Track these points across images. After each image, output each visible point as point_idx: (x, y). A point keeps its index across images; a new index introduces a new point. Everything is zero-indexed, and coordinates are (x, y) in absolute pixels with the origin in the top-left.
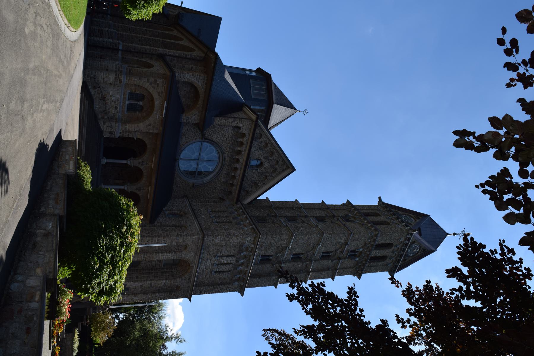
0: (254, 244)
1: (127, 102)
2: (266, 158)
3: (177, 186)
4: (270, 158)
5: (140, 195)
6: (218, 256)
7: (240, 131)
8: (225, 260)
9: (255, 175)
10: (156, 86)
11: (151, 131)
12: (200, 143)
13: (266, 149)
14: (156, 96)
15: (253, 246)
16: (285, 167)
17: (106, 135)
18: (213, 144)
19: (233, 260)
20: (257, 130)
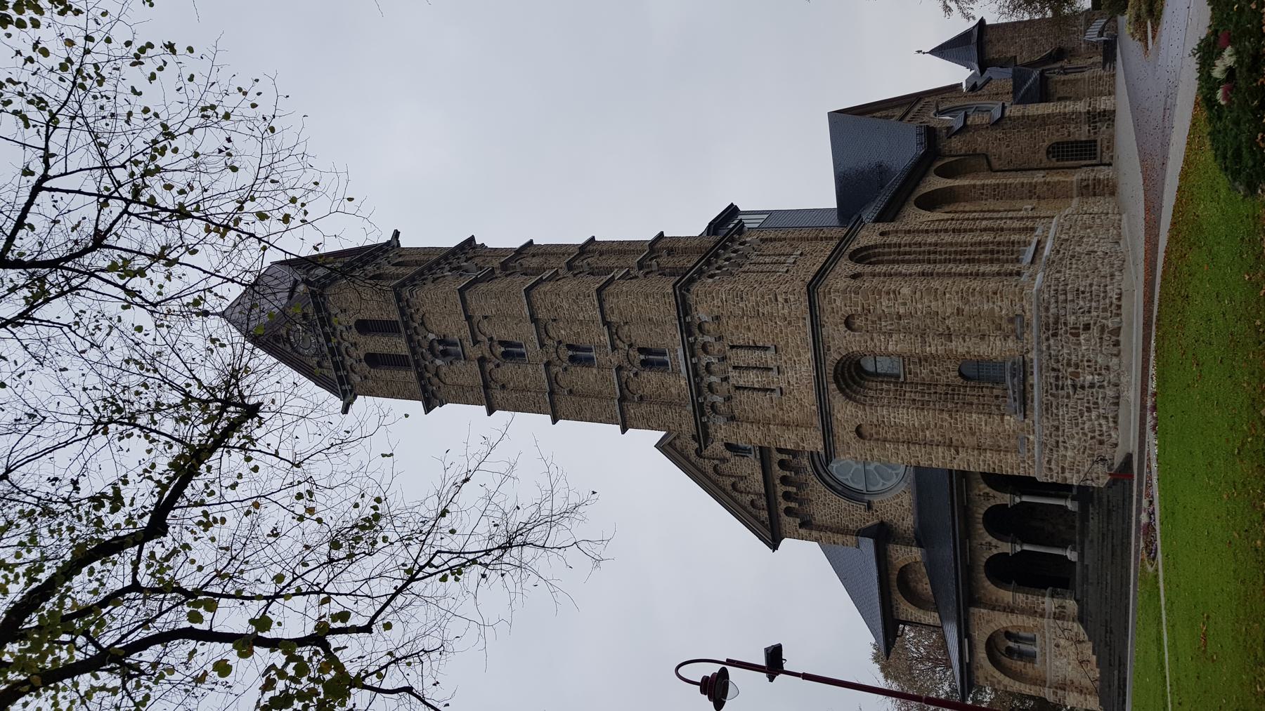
2: (724, 460)
5: (983, 486)
6: (773, 390)
7: (798, 521)
8: (752, 378)
12: (872, 489)
13: (733, 480)
15: (705, 419)
16: (678, 442)
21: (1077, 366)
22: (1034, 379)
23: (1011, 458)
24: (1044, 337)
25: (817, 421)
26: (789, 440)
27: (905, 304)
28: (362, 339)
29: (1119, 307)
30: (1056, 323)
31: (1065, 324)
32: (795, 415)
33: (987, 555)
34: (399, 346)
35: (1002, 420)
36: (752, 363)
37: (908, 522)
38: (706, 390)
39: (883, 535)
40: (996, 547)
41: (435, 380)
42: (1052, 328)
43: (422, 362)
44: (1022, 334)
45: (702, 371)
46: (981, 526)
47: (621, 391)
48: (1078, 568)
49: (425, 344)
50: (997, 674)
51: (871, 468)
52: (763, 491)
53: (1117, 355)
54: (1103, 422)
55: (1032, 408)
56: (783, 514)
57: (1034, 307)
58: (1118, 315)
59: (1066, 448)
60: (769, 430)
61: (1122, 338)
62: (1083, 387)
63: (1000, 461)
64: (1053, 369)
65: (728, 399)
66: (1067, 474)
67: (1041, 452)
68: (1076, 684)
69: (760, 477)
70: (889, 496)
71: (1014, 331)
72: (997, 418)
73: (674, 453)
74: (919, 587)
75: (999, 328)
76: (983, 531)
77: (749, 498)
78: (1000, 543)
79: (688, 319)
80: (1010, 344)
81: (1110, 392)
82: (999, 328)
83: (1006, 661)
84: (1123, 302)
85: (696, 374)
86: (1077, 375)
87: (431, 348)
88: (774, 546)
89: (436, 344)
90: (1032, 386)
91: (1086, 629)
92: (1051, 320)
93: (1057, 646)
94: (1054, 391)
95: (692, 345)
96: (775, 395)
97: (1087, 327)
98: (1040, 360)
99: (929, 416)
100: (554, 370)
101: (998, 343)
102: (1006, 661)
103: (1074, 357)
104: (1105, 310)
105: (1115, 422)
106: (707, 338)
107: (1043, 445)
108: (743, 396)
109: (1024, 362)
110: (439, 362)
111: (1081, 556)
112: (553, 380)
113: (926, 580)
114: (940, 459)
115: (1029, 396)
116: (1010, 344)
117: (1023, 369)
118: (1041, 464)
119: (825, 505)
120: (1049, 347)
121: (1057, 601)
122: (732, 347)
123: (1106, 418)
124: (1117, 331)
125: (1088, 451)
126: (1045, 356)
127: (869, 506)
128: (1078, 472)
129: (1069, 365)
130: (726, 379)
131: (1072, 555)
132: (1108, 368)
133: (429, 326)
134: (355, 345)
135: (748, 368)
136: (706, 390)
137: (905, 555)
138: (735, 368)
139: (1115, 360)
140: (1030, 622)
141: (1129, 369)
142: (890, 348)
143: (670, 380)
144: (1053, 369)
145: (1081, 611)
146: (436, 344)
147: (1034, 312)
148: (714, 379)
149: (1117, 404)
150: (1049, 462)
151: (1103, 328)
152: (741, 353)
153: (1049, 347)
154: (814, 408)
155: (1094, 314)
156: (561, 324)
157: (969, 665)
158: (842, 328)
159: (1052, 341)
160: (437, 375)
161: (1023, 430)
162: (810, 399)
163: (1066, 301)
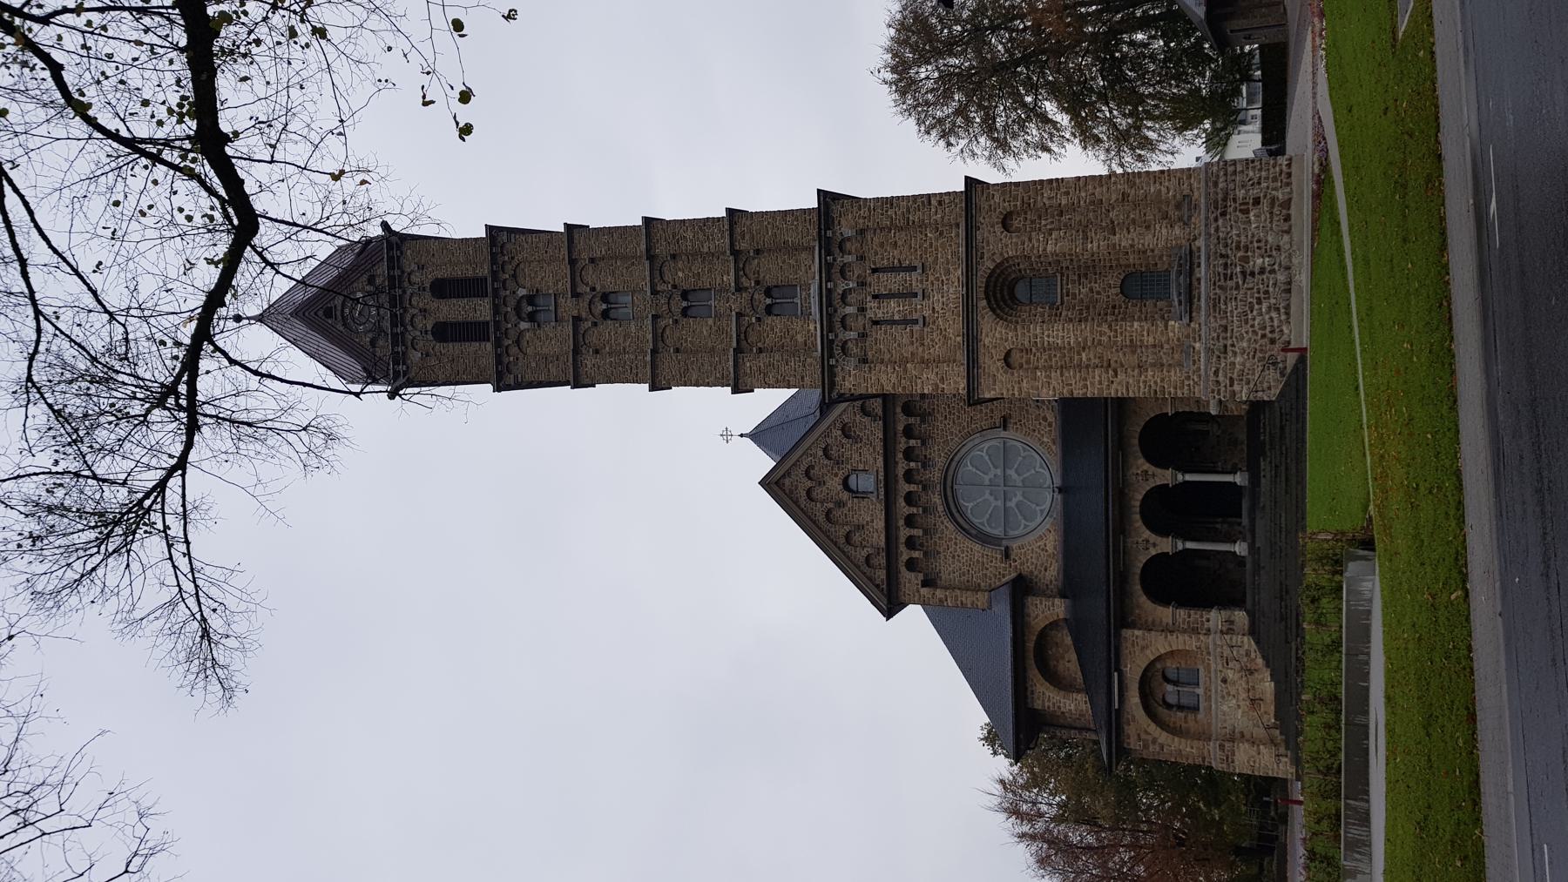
0: (831, 367)
1: (1200, 691)
2: (840, 504)
3: (1045, 419)
4: (831, 505)
5: (1141, 460)
6: (916, 322)
7: (921, 577)
8: (894, 308)
9: (856, 456)
10: (1143, 736)
11: (1137, 632)
12: (1012, 533)
13: (847, 528)
14: (1140, 713)
15: (833, 362)
16: (787, 481)
17: (1240, 617)
18: (980, 532)
19: (875, 310)
20: (884, 577)
21: (1247, 249)
22: (1202, 272)
23: (1175, 376)
24: (1212, 217)
25: (961, 356)
26: (926, 382)
27: (1067, 193)
28: (434, 304)
29: (1289, 175)
30: (1225, 199)
31: (1235, 200)
32: (937, 350)
33: (1143, 559)
34: (481, 310)
35: (1166, 327)
36: (895, 288)
37: (1052, 573)
38: (838, 325)
39: (1022, 588)
40: (1154, 545)
41: (514, 350)
42: (1220, 207)
43: (504, 326)
44: (1190, 217)
45: (837, 301)
46: (1138, 517)
47: (738, 342)
48: (1249, 566)
49: (512, 302)
50: (1153, 728)
51: (1012, 504)
52: (883, 544)
53: (1288, 232)
54: (1274, 315)
55: (1199, 308)
56: (903, 569)
57: (1203, 183)
58: (1288, 184)
59: (1235, 353)
60: (905, 370)
61: (1293, 212)
62: (1252, 274)
63: (1162, 380)
64: (1222, 256)
65: (863, 336)
66: (1236, 388)
67: (1208, 361)
68: (1248, 736)
69: (880, 524)
70: (1031, 538)
71: (1180, 219)
72: (1161, 324)
73: (780, 493)
74: (1061, 668)
75: (1166, 216)
76: (1139, 524)
77: (864, 553)
78: (1159, 539)
79: (829, 233)
80: (1177, 231)
81: (1281, 277)
82: (1166, 216)
83: (1162, 711)
84: (1294, 169)
85: (829, 304)
86: (1245, 259)
87: (518, 309)
88: (889, 613)
89: (524, 304)
90: (1199, 280)
91: (1257, 643)
92: (1220, 196)
93: (1224, 681)
94: (1222, 283)
95: (829, 266)
96: (916, 328)
97: (1257, 201)
98: (1207, 246)
99: (1087, 331)
100: (663, 323)
101: (1164, 231)
102: (1162, 711)
103: (1243, 238)
104: (1275, 180)
105: (1287, 314)
106: (849, 259)
107: (1209, 351)
108: (879, 333)
109: (1191, 252)
110: (524, 325)
111: (1252, 547)
112: (659, 336)
113: (1074, 657)
114: (1096, 385)
115: (1195, 293)
116: (1177, 231)
117: (1189, 261)
118: (1207, 375)
119: (958, 556)
120: (1217, 229)
121: (1225, 614)
122: (874, 271)
123: (1278, 309)
124: (1287, 204)
125: (1259, 354)
126: (1213, 240)
127: (1007, 554)
128: (1248, 383)
129: (1238, 248)
130: (862, 310)
131: (1240, 548)
132: (1278, 248)
133: (521, 280)
134: (424, 311)
135: (891, 296)
136: (838, 325)
137: (1047, 610)
138: (875, 297)
139: (1286, 238)
140: (1191, 643)
141: (1300, 249)
142: (1049, 248)
143: (797, 325)
144: (1222, 256)
145: (1253, 624)
146: (524, 304)
147: (1202, 190)
148: (850, 310)
149: (1289, 291)
150: (1216, 373)
151: (1273, 200)
152: (883, 276)
153: (1217, 229)
154: (959, 339)
155: (1264, 185)
156: (680, 265)
157: (1118, 712)
158: (998, 228)
159: (1220, 222)
160: (518, 342)
161: (1188, 336)
162: (954, 328)
163: (1235, 172)
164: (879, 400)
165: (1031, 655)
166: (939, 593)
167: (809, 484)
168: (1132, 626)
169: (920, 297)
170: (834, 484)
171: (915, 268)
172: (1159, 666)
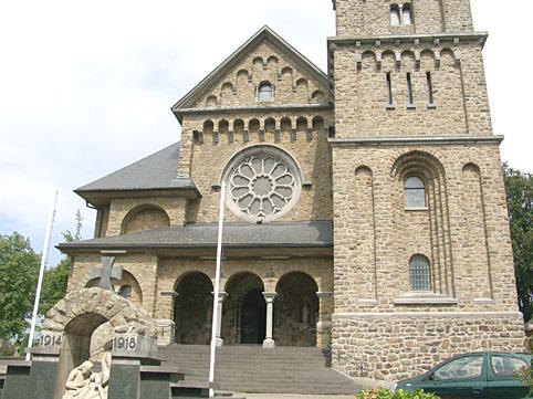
8: (399, 85)
11: (155, 267)
46: (240, 270)
125: (369, 356)
138: (408, 75)
164: (311, 236)
165: (145, 202)
166: (189, 143)
167: (265, 59)
168: (160, 266)
169: (410, 106)
170: (265, 76)
171: (431, 102)
172: (132, 282)
